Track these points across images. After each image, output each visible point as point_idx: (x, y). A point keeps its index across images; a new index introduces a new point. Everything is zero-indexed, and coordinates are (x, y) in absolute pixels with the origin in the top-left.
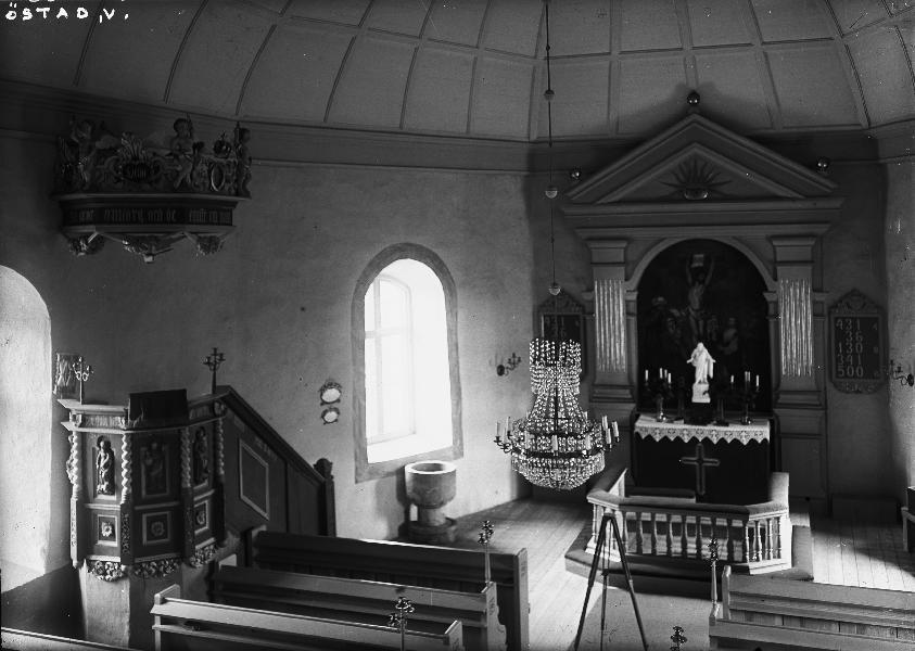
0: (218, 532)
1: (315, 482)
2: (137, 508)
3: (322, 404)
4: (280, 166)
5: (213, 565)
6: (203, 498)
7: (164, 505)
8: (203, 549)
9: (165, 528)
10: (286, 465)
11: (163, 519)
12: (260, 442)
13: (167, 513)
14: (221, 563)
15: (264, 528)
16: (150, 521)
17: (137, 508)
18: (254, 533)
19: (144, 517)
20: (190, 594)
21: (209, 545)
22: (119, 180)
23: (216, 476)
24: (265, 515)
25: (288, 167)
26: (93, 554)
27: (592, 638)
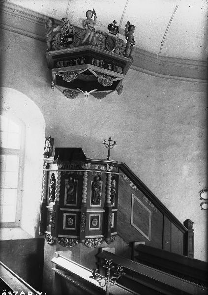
0: (105, 231)
1: (183, 231)
2: (61, 209)
3: (200, 199)
4: (182, 80)
5: (100, 249)
6: (95, 210)
7: (73, 210)
8: (94, 239)
9: (74, 222)
10: (164, 216)
11: (73, 217)
12: (147, 199)
13: (75, 215)
14: (103, 249)
15: (144, 243)
16: (68, 217)
17: (61, 209)
18: (136, 244)
19: (65, 215)
20: (75, 259)
21: (99, 238)
22: (61, 45)
23: (106, 203)
24: (148, 238)
25: (186, 81)
26: (46, 230)
27: (201, 68)
